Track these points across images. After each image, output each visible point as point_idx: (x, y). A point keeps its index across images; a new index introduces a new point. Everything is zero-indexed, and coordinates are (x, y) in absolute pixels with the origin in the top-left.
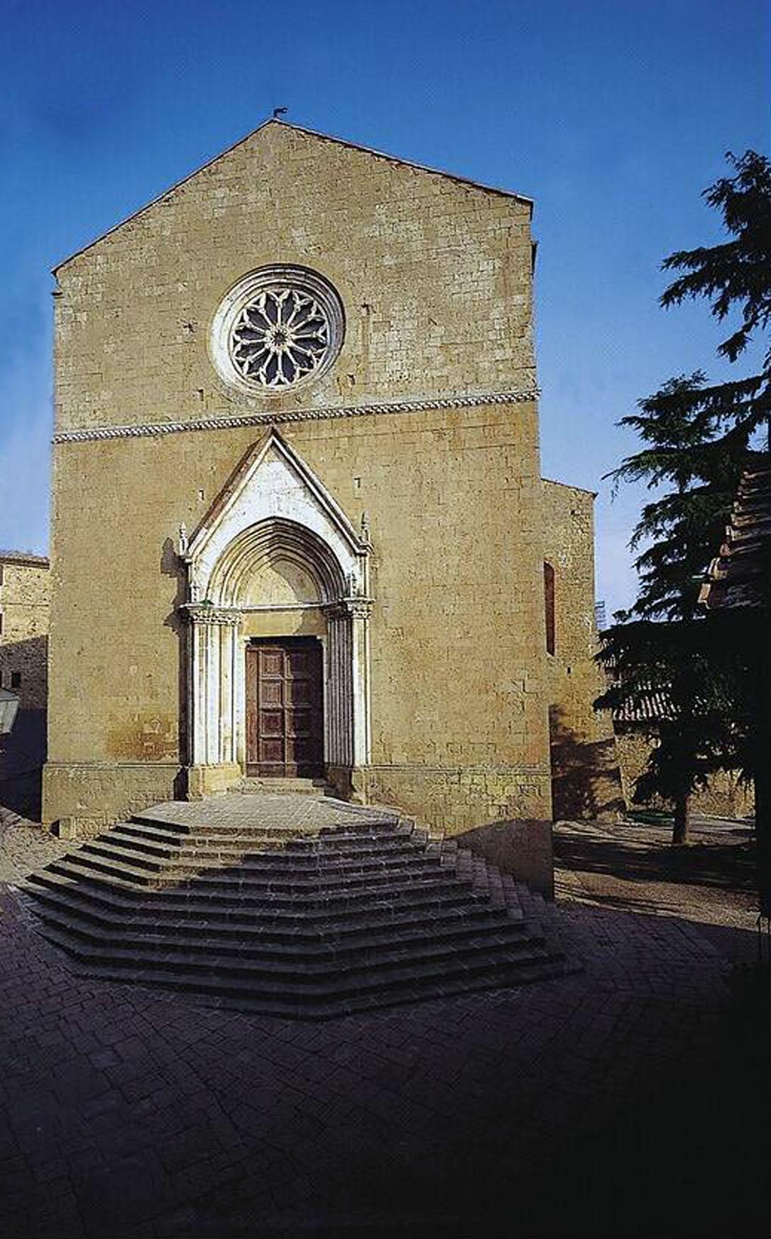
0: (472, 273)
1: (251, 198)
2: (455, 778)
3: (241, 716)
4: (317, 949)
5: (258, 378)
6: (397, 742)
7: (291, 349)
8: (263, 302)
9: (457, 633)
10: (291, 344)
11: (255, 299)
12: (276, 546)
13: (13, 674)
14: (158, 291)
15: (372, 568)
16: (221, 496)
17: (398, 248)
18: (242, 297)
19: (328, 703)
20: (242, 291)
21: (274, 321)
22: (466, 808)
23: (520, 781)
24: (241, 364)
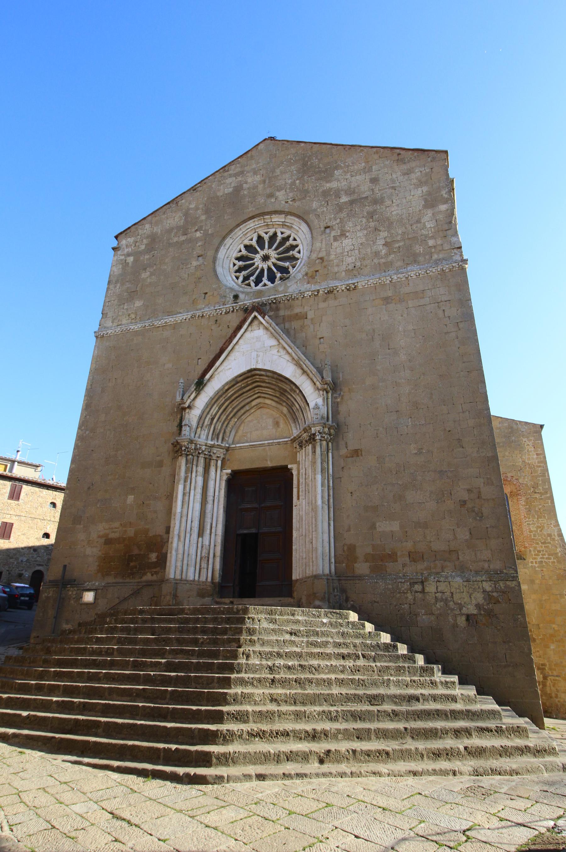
0: (406, 198)
1: (250, 180)
2: (418, 587)
3: (219, 539)
4: (529, 762)
5: (249, 285)
6: (360, 552)
7: (274, 265)
8: (255, 239)
9: (413, 448)
10: (274, 260)
11: (250, 238)
12: (256, 396)
13: (18, 498)
14: (183, 238)
15: (334, 403)
16: (504, 827)
17: (350, 191)
18: (241, 236)
19: (240, 447)
20: (241, 232)
21: (269, 269)
22: (433, 618)
23: (487, 586)
24: (237, 278)
